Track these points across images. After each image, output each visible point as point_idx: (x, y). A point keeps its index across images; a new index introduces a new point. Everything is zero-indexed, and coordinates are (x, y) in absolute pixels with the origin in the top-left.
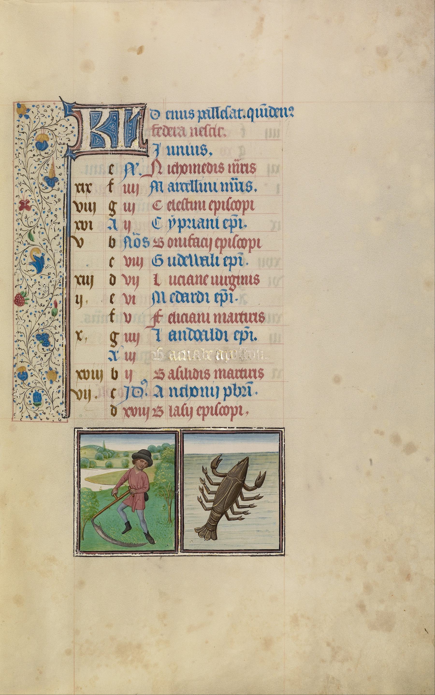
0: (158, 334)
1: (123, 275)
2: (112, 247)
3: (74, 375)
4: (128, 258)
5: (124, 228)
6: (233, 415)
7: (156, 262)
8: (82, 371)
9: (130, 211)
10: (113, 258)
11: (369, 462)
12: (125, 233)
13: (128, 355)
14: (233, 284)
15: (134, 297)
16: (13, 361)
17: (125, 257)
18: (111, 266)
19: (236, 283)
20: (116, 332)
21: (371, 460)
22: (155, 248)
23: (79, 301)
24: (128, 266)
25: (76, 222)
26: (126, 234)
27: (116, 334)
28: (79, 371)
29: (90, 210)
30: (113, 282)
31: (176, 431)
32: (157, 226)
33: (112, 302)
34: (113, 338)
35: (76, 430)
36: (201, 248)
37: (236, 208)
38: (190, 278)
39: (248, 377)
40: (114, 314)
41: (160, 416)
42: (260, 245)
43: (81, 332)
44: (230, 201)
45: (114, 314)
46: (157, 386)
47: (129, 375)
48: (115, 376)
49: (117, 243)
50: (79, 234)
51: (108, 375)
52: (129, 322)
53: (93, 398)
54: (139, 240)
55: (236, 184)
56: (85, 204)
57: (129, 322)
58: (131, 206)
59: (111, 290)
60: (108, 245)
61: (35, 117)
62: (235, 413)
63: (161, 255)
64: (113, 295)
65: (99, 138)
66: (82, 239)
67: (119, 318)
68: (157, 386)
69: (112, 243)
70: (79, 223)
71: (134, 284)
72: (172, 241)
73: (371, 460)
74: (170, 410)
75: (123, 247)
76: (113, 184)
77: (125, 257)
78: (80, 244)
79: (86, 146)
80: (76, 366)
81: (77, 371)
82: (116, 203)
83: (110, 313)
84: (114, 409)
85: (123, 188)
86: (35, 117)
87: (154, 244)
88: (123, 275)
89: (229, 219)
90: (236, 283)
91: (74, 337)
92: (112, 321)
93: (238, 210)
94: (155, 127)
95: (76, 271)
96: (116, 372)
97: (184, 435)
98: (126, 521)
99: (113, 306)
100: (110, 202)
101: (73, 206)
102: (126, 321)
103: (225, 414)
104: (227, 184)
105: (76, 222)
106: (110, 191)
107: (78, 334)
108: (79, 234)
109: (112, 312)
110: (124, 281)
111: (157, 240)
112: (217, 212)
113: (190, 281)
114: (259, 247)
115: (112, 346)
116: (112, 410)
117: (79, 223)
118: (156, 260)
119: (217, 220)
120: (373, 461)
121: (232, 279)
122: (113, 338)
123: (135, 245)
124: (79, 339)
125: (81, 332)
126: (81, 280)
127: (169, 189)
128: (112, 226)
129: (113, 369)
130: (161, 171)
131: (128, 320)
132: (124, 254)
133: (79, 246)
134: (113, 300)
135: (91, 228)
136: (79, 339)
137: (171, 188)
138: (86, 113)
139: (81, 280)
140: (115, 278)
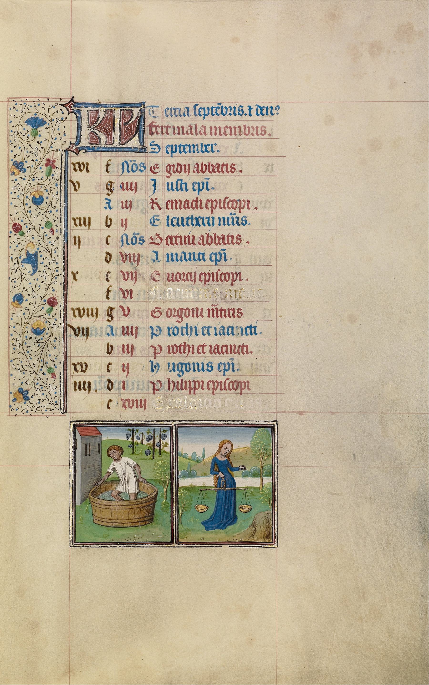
0: (154, 185)
2: (109, 227)
5: (122, 334)
6: (233, 281)
8: (77, 309)
9: (127, 208)
10: (109, 272)
12: (122, 231)
13: (124, 203)
15: (131, 202)
16: (9, 239)
17: (122, 272)
21: (354, 455)
22: (151, 244)
23: (78, 241)
24: (125, 280)
25: (74, 364)
26: (122, 233)
29: (92, 315)
30: (108, 260)
33: (107, 280)
35: (72, 424)
37: (233, 207)
38: (187, 202)
40: (110, 291)
43: (77, 272)
44: (227, 200)
45: (110, 291)
46: (154, 251)
47: (125, 223)
48: (108, 223)
50: (75, 176)
51: (102, 314)
53: (92, 391)
54: (136, 238)
55: (233, 219)
58: (129, 203)
59: (107, 178)
61: (45, 304)
62: (235, 278)
64: (111, 400)
65: (96, 137)
68: (154, 251)
69: (108, 258)
70: (76, 311)
71: (132, 279)
73: (354, 455)
74: (167, 219)
75: (121, 173)
76: (109, 165)
77: (121, 253)
79: (85, 142)
80: (73, 304)
82: (114, 183)
84: (110, 384)
85: (121, 221)
86: (45, 304)
87: (151, 241)
89: (223, 363)
90: (184, 369)
91: (70, 276)
92: (108, 298)
93: (235, 209)
94: (154, 124)
96: (111, 220)
97: (179, 429)
101: (70, 331)
102: (125, 315)
103: (224, 274)
105: (74, 364)
107: (74, 275)
109: (108, 163)
110: (122, 295)
111: (153, 237)
112: (214, 210)
113: (186, 206)
117: (76, 311)
119: (213, 218)
123: (132, 243)
124: (75, 279)
125: (77, 272)
126: (77, 222)
128: (107, 206)
131: (126, 313)
134: (110, 406)
136: (75, 279)
138: (84, 111)
139: (77, 222)
140: (112, 384)
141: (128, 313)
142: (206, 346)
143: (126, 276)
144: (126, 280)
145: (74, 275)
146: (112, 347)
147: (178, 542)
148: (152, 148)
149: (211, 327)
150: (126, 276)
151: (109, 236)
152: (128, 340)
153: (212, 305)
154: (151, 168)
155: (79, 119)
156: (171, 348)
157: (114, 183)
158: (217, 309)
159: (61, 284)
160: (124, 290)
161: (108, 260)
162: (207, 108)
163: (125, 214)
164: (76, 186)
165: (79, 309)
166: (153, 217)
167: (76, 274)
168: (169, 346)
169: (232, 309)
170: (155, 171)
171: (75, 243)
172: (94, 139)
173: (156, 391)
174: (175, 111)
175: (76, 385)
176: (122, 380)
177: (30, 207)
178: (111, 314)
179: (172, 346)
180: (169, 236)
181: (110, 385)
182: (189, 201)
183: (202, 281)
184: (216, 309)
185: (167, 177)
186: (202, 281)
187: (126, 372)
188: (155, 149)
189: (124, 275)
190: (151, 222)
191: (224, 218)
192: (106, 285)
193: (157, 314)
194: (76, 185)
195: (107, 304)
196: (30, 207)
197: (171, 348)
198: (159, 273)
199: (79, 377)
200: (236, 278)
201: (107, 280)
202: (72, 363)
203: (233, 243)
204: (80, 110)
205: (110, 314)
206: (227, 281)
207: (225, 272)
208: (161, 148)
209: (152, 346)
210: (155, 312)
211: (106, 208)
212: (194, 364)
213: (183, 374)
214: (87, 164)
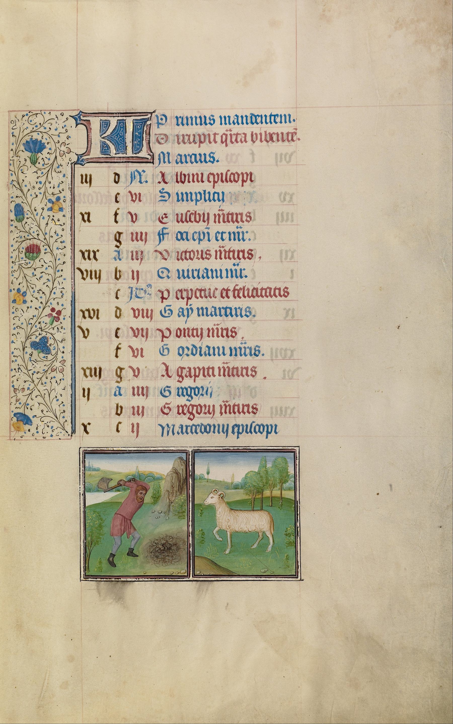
1: (130, 347)
3: (79, 315)
4: (135, 329)
7: (163, 352)
11: (389, 487)
14: (191, 413)
18: (117, 298)
19: (194, 412)
20: (122, 367)
21: (391, 486)
23: (87, 393)
25: (82, 311)
27: (120, 234)
28: (84, 310)
30: (118, 315)
31: (190, 577)
32: (164, 354)
33: (117, 336)
34: (119, 373)
36: (204, 163)
39: (244, 142)
41: (167, 414)
42: (277, 431)
45: (118, 214)
46: (164, 363)
47: (136, 275)
49: (122, 179)
50: (86, 324)
52: (137, 376)
56: (91, 272)
57: (134, 222)
59: (115, 189)
60: (114, 277)
63: (170, 306)
66: (88, 330)
67: (126, 332)
69: (119, 410)
71: (143, 336)
72: (181, 331)
73: (391, 486)
76: (120, 348)
77: (133, 309)
78: (86, 335)
81: (83, 368)
82: (122, 233)
83: (114, 213)
84: (118, 311)
88: (130, 347)
90: (194, 412)
92: (116, 222)
95: (81, 245)
96: (121, 408)
98: (132, 547)
99: (117, 205)
100: (117, 368)
103: (234, 175)
104: (234, 233)
105: (81, 214)
106: (117, 356)
107: (85, 427)
108: (86, 324)
114: (276, 433)
115: (117, 382)
116: (116, 312)
118: (163, 349)
120: (393, 486)
121: (189, 389)
122: (119, 373)
126: (88, 372)
127: (178, 314)
129: (117, 405)
130: (169, 275)
131: (136, 374)
132: (130, 189)
133: (85, 337)
135: (98, 318)
137: (180, 314)
138: (95, 123)
139: (88, 372)
140: (120, 310)
141: (138, 374)
142: (230, 290)
143: (136, 332)
144: (134, 201)
145: (85, 427)
146: (118, 175)
147: (194, 575)
148: (161, 196)
149: (218, 134)
150: (136, 332)
151: (118, 194)
152: (139, 401)
153: (224, 363)
154: (161, 312)
155: (88, 130)
156: (181, 391)
157: (122, 233)
158: (228, 367)
159: (69, 317)
160: (133, 193)
161: (117, 180)
162: (216, 174)
163: (135, 265)
164: (86, 333)
165: (88, 310)
166: (163, 347)
167: (88, 426)
168: (178, 406)
169: (245, 368)
170: (163, 221)
171: (84, 396)
172: (105, 149)
173: (164, 300)
174: (186, 254)
175: (83, 179)
176: (130, 250)
177: (42, 412)
178: (119, 240)
179: (181, 406)
180: (179, 290)
181: (118, 275)
182: (196, 154)
183: (210, 182)
184: (227, 367)
185: (179, 381)
186: (210, 182)
187: (135, 433)
188: (164, 197)
189: (133, 351)
190: (161, 393)
191: (235, 348)
192: (116, 342)
193: (167, 393)
194: (86, 332)
195: (117, 363)
196: (42, 412)
197: (181, 391)
198: (166, 216)
199: (86, 265)
200: (247, 179)
201: (117, 336)
202: (80, 309)
203: (249, 412)
204: (89, 121)
205: (118, 239)
206: (237, 182)
207: (234, 172)
208: (172, 332)
209: (159, 291)
210: (165, 391)
211: (115, 259)
212: (201, 124)
213: (194, 417)
214: (98, 310)
